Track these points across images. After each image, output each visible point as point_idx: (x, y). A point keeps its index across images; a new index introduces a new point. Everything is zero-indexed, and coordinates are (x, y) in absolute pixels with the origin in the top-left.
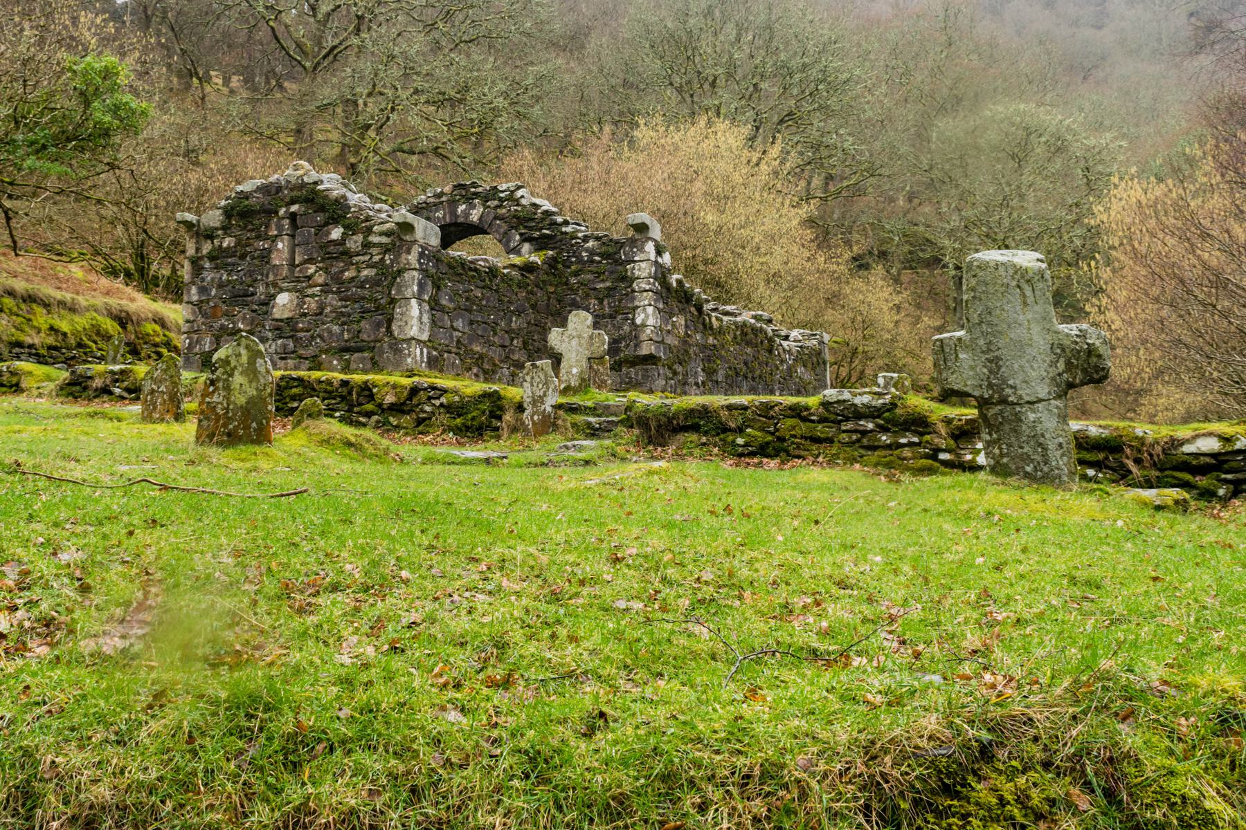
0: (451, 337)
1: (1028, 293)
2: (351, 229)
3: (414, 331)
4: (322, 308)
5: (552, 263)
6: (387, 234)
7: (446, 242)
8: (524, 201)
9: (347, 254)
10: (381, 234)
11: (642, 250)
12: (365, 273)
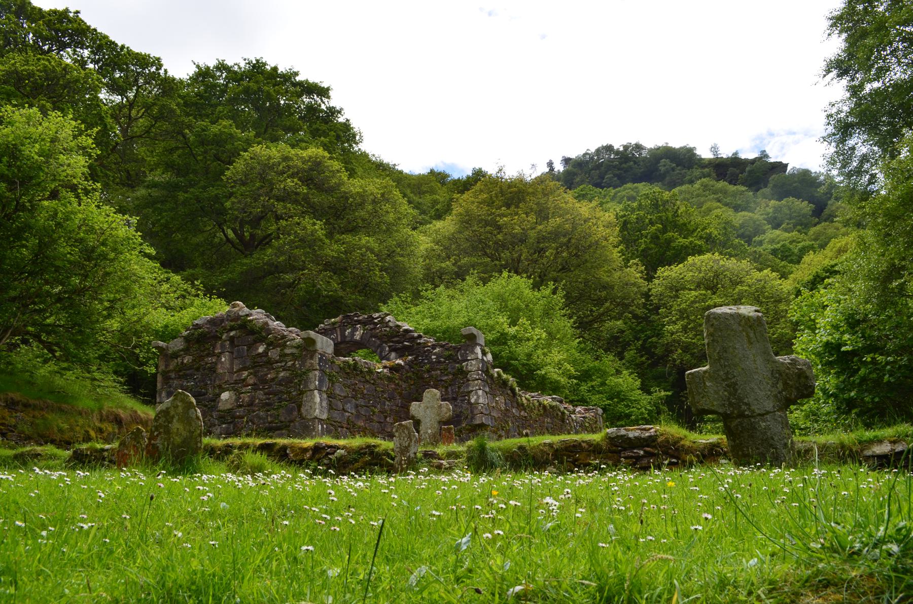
0: (343, 415)
1: (752, 335)
2: (270, 344)
3: (317, 413)
4: (252, 399)
5: (410, 364)
6: (298, 347)
7: (338, 352)
8: (391, 324)
9: (270, 363)
10: (292, 347)
11: (473, 352)
12: (282, 374)
